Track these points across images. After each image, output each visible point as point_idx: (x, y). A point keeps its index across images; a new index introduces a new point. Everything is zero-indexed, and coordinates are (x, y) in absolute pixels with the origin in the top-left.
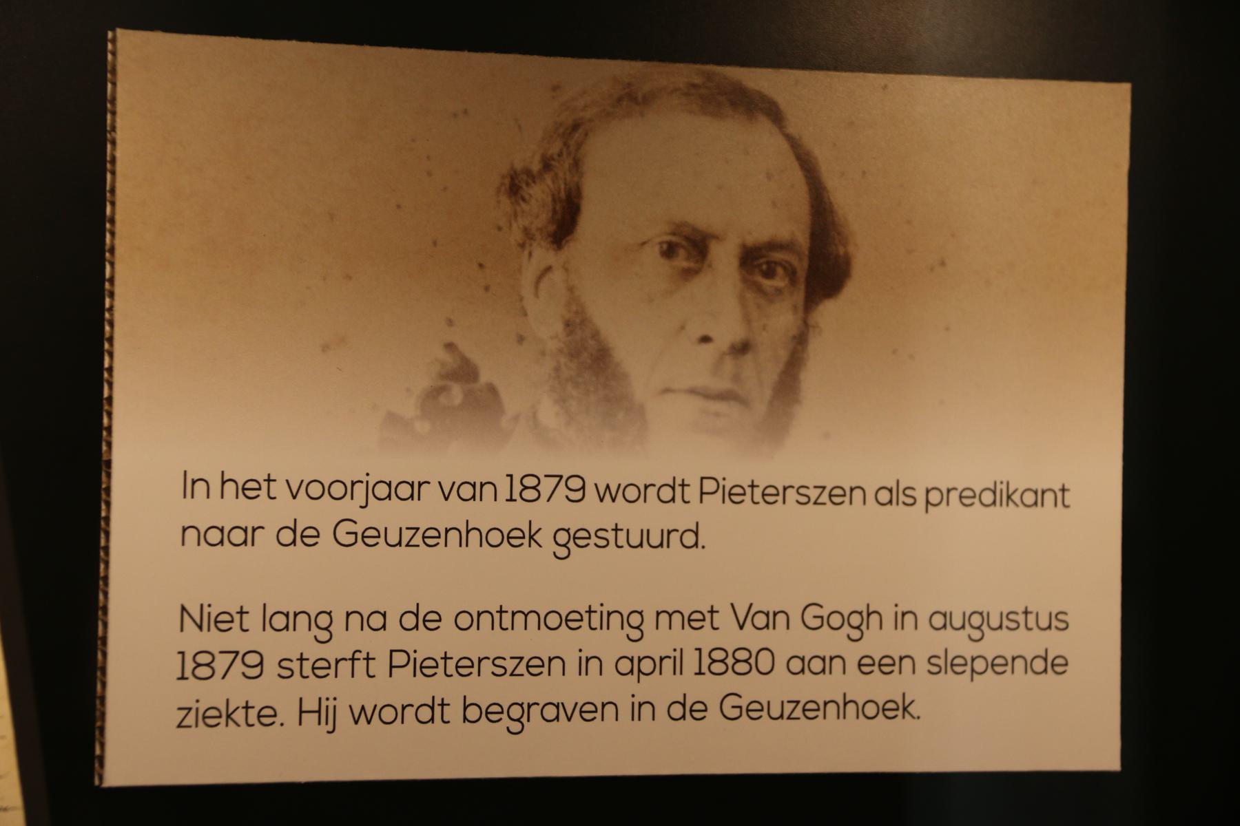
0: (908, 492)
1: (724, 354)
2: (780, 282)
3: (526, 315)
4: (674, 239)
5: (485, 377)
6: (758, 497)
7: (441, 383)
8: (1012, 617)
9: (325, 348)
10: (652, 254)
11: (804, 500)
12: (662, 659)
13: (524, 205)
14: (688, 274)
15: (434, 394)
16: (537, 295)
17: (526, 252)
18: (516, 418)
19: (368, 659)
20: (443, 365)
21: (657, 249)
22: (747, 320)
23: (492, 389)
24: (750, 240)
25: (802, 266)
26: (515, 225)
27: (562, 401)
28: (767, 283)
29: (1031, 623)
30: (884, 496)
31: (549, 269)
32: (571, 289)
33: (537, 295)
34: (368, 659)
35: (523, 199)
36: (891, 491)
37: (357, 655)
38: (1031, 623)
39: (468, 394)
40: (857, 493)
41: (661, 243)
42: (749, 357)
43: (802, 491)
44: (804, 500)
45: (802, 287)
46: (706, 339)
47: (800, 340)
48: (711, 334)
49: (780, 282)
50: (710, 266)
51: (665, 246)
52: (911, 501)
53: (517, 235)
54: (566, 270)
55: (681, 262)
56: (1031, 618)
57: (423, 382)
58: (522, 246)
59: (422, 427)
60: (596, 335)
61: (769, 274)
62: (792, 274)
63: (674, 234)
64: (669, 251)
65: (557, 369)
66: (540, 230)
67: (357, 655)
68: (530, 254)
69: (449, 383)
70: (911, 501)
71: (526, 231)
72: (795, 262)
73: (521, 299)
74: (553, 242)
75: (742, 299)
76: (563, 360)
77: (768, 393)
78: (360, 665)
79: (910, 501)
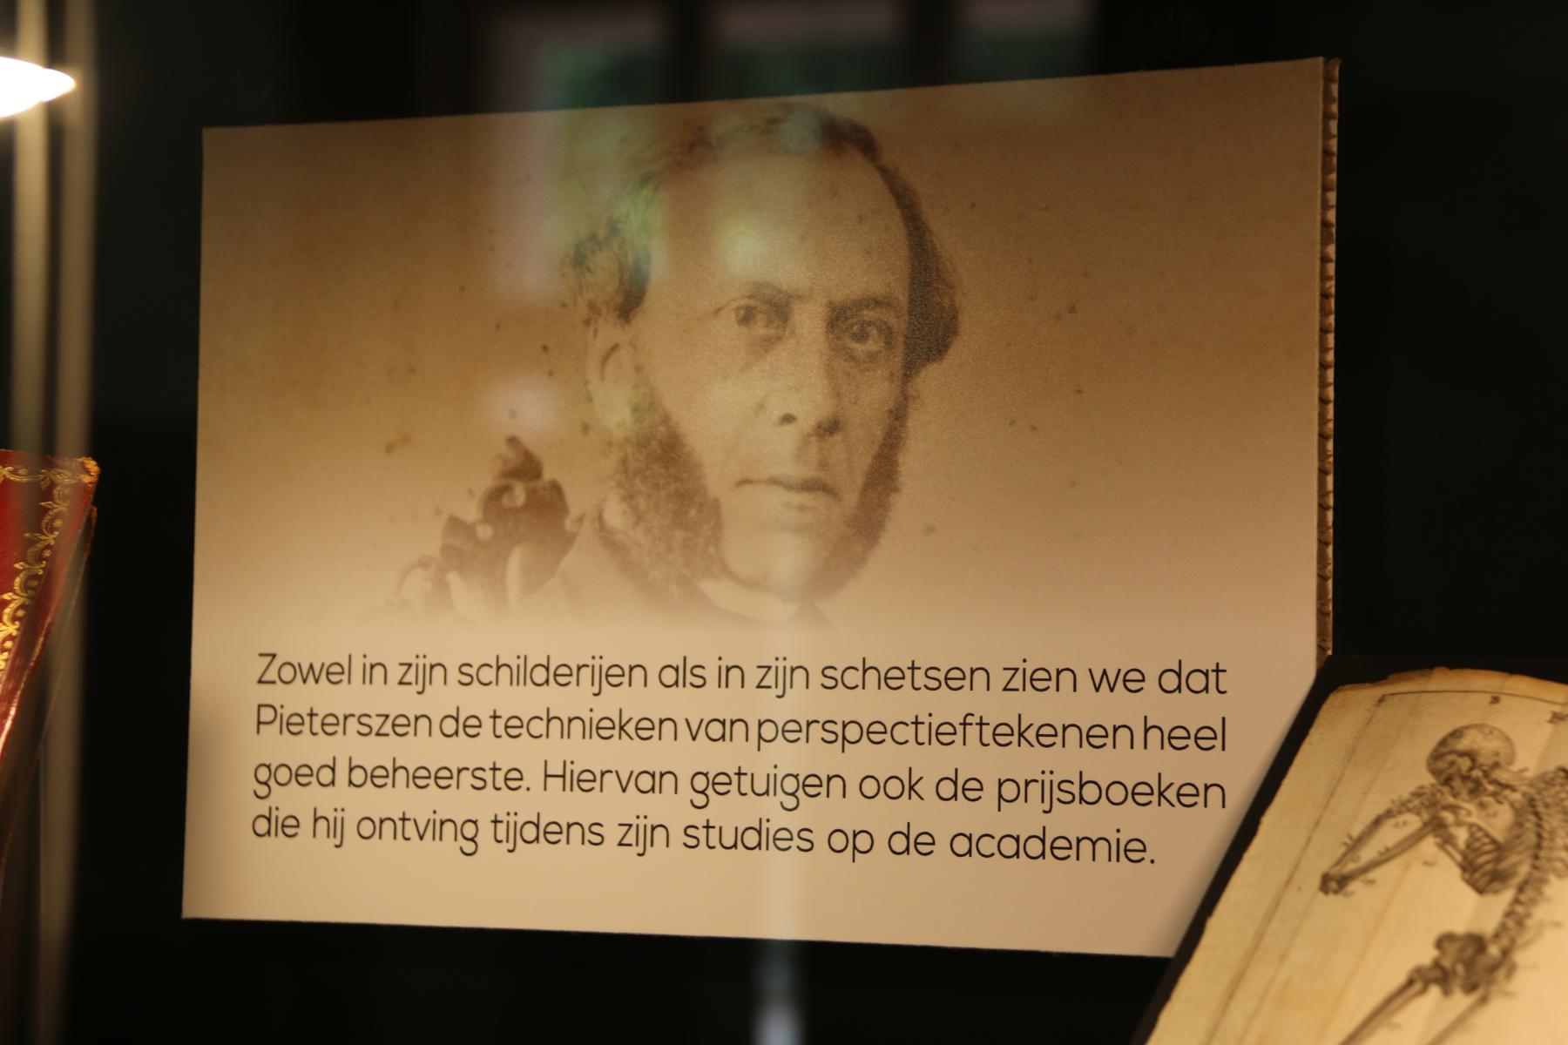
0: (697, 671)
1: (809, 435)
2: (872, 345)
3: (591, 400)
4: (752, 302)
5: (548, 475)
6: (317, 728)
7: (504, 482)
8: (1065, 786)
9: (390, 448)
10: (729, 318)
11: (366, 730)
12: (1027, 783)
13: (588, 275)
14: (768, 343)
15: (496, 495)
16: (602, 378)
17: (592, 328)
18: (581, 519)
19: (981, 724)
20: (505, 462)
21: (733, 316)
22: (837, 395)
23: (556, 488)
24: (840, 296)
25: (899, 324)
26: (580, 300)
27: (629, 497)
28: (860, 349)
29: (714, 841)
30: (669, 676)
31: (615, 347)
32: (638, 369)
33: (602, 378)
34: (981, 724)
35: (589, 270)
36: (677, 670)
37: (969, 719)
38: (714, 841)
39: (531, 493)
40: (638, 673)
41: (738, 309)
42: (838, 437)
43: (364, 720)
44: (366, 730)
45: (900, 351)
46: (788, 419)
47: (898, 416)
48: (793, 412)
49: (872, 345)
50: (793, 332)
51: (742, 312)
52: (700, 682)
53: (582, 311)
54: (635, 348)
55: (760, 329)
56: (714, 833)
57: (485, 481)
58: (587, 322)
59: (485, 532)
60: (666, 420)
61: (862, 337)
62: (888, 335)
63: (750, 297)
64: (747, 317)
65: (624, 461)
66: (607, 303)
67: (969, 719)
68: (596, 331)
69: (511, 481)
70: (700, 682)
71: (592, 307)
72: (893, 322)
73: (586, 383)
74: (620, 316)
75: (830, 371)
76: (630, 450)
77: (860, 481)
78: (973, 731)
79: (699, 682)
